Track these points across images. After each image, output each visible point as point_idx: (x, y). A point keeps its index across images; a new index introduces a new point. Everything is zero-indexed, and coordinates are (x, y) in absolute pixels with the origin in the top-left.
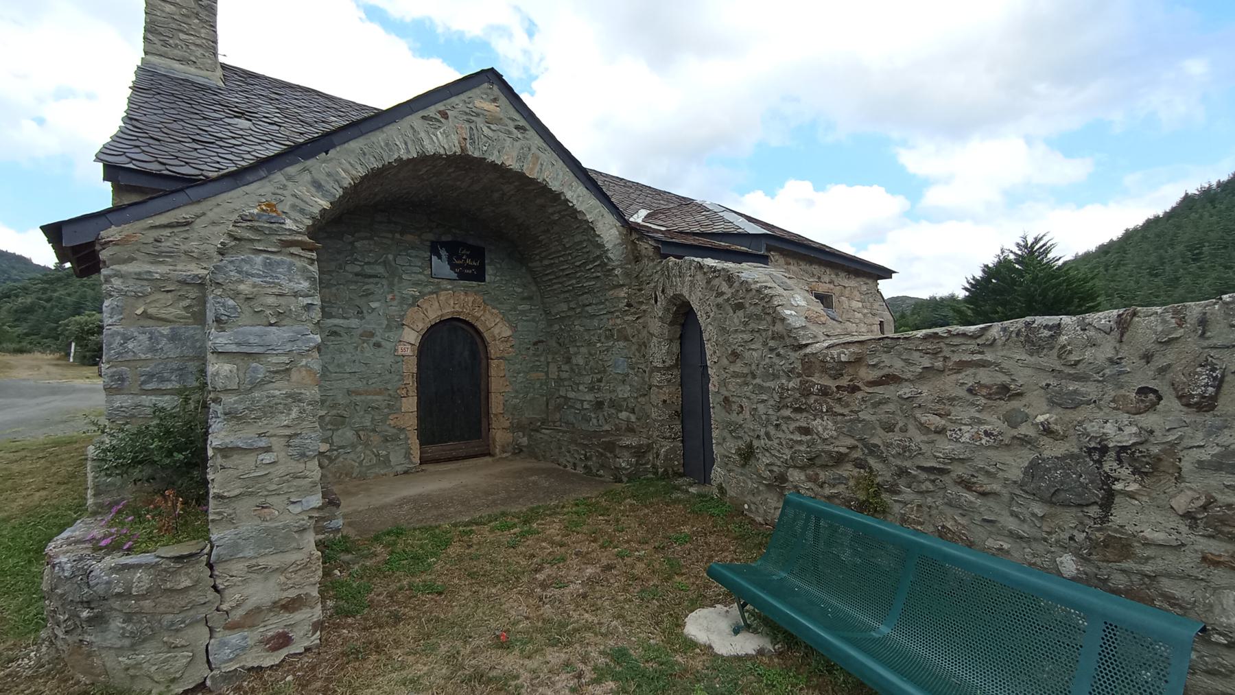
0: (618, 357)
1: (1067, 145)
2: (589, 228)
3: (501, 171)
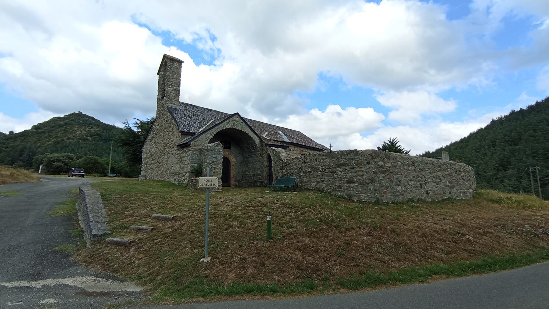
0: (258, 165)
1: (446, 96)
2: (253, 140)
3: (238, 130)
